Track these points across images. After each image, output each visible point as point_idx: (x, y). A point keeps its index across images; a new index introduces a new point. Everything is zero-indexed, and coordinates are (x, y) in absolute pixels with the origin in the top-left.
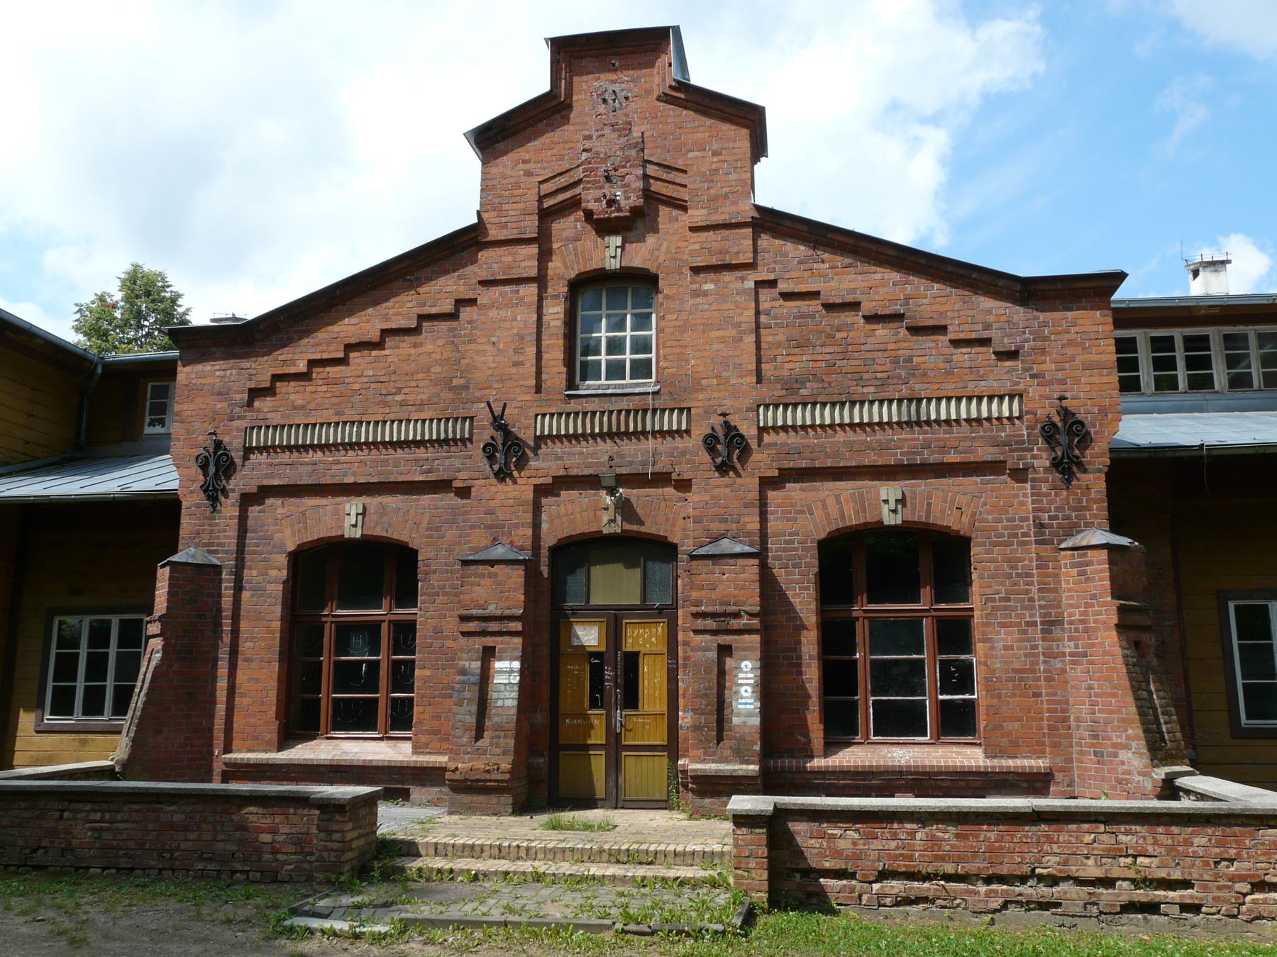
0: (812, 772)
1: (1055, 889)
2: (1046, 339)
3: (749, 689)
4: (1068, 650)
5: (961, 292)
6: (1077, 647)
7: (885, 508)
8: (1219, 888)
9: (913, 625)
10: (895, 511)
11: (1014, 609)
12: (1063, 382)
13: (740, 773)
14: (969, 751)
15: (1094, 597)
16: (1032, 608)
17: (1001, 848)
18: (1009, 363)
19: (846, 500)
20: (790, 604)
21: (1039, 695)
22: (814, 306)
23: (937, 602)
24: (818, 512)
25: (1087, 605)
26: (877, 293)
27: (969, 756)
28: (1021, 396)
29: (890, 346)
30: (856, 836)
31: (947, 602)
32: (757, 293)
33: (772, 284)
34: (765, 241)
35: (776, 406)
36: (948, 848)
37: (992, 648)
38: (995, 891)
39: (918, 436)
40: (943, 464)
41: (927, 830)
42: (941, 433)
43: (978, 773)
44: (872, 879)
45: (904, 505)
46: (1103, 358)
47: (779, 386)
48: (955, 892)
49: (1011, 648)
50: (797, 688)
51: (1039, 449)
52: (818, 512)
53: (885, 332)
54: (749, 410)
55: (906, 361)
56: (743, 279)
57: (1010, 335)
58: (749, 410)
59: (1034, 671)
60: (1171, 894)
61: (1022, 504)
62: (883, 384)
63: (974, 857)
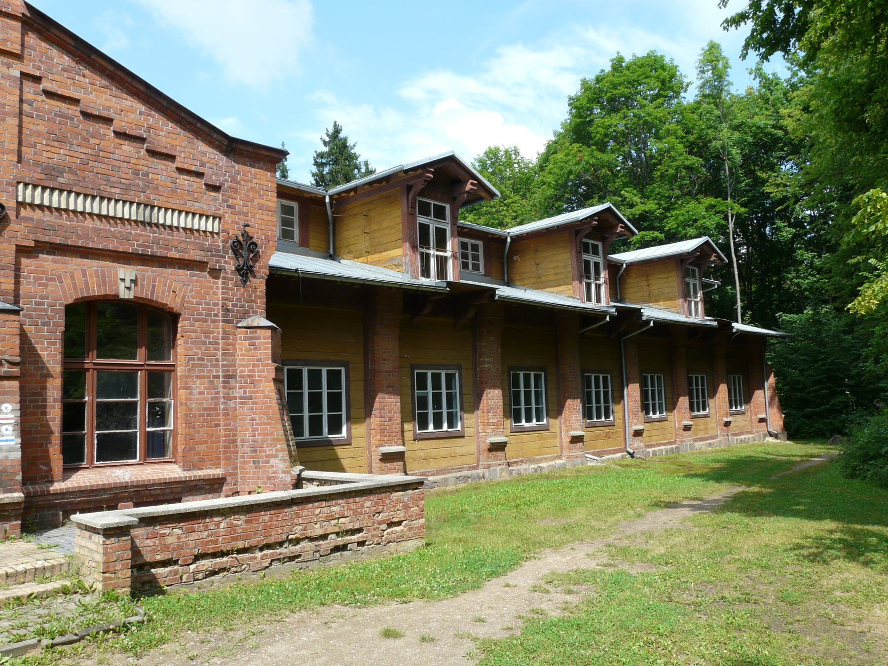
0: (54, 494)
1: (298, 547)
2: (238, 183)
3: (10, 428)
4: (238, 395)
5: (187, 134)
6: (245, 393)
7: (122, 286)
8: (374, 530)
9: (130, 376)
10: (129, 288)
11: (206, 366)
12: (246, 214)
13: (6, 501)
14: (168, 467)
15: (259, 360)
16: (218, 366)
17: (271, 525)
18: (213, 194)
19: (91, 275)
20: (39, 356)
21: (217, 425)
22: (73, 111)
23: (149, 359)
24: (67, 282)
25: (254, 366)
26: (126, 116)
27: (170, 471)
28: (220, 219)
29: (133, 161)
30: (180, 532)
31: (156, 359)
32: (21, 83)
33: (37, 79)
34: (32, 39)
35: (35, 187)
36: (240, 531)
37: (191, 393)
38: (266, 555)
39: (150, 234)
40: (167, 257)
41: (227, 520)
42: (166, 235)
43: (180, 482)
44: (190, 562)
45: (136, 285)
46: (270, 204)
47: (39, 170)
48: (243, 560)
49: (203, 393)
50: (42, 426)
51: (229, 257)
52: (67, 282)
53: (131, 149)
54: (8, 184)
55: (143, 175)
56: (9, 66)
57: (216, 174)
58: (8, 184)
59: (216, 409)
60: (353, 537)
61: (215, 294)
62: (126, 189)
63: (255, 534)
